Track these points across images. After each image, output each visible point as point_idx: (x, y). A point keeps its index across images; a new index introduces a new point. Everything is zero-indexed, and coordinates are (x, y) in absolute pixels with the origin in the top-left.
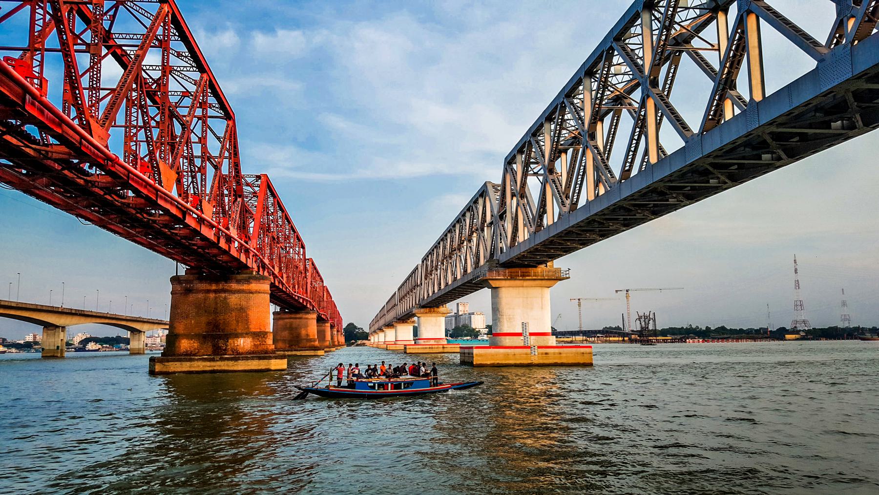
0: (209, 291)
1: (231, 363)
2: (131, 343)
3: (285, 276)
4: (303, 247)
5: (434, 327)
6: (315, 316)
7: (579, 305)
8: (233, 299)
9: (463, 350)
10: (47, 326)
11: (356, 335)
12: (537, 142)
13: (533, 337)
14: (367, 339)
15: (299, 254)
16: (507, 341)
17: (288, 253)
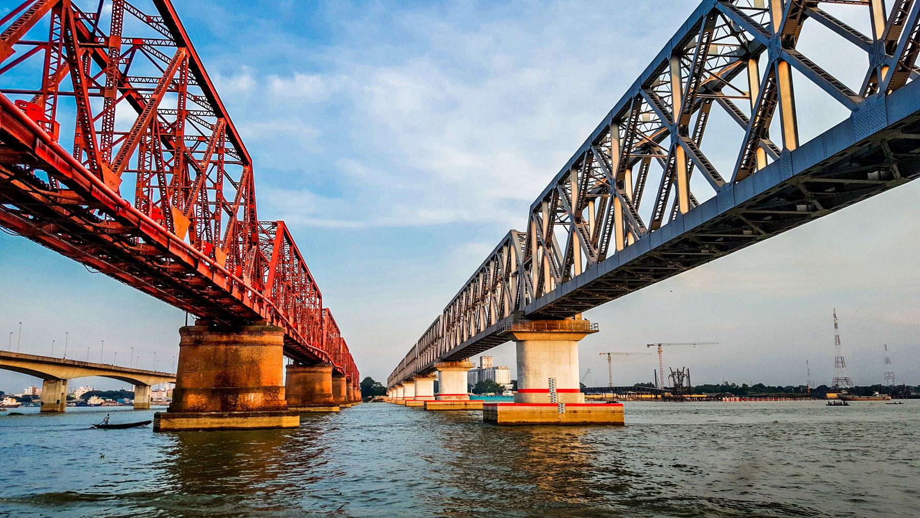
0: (219, 343)
1: (240, 420)
2: (136, 398)
3: (299, 327)
4: (320, 297)
5: (456, 382)
6: (330, 370)
7: (609, 359)
8: (245, 352)
9: (486, 408)
10: (48, 378)
11: (373, 390)
12: (564, 190)
13: (560, 394)
14: (385, 395)
15: (315, 303)
16: (533, 398)
17: (304, 302)
